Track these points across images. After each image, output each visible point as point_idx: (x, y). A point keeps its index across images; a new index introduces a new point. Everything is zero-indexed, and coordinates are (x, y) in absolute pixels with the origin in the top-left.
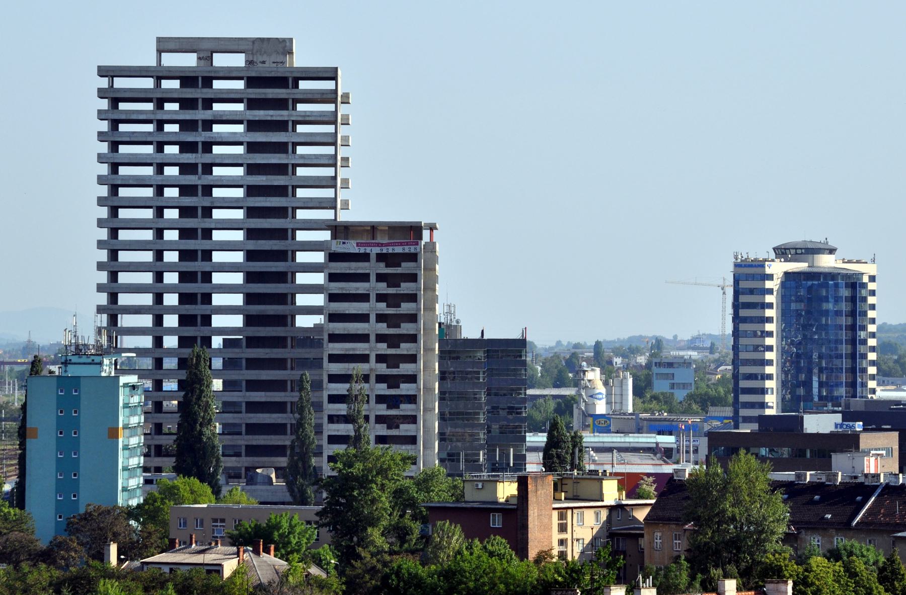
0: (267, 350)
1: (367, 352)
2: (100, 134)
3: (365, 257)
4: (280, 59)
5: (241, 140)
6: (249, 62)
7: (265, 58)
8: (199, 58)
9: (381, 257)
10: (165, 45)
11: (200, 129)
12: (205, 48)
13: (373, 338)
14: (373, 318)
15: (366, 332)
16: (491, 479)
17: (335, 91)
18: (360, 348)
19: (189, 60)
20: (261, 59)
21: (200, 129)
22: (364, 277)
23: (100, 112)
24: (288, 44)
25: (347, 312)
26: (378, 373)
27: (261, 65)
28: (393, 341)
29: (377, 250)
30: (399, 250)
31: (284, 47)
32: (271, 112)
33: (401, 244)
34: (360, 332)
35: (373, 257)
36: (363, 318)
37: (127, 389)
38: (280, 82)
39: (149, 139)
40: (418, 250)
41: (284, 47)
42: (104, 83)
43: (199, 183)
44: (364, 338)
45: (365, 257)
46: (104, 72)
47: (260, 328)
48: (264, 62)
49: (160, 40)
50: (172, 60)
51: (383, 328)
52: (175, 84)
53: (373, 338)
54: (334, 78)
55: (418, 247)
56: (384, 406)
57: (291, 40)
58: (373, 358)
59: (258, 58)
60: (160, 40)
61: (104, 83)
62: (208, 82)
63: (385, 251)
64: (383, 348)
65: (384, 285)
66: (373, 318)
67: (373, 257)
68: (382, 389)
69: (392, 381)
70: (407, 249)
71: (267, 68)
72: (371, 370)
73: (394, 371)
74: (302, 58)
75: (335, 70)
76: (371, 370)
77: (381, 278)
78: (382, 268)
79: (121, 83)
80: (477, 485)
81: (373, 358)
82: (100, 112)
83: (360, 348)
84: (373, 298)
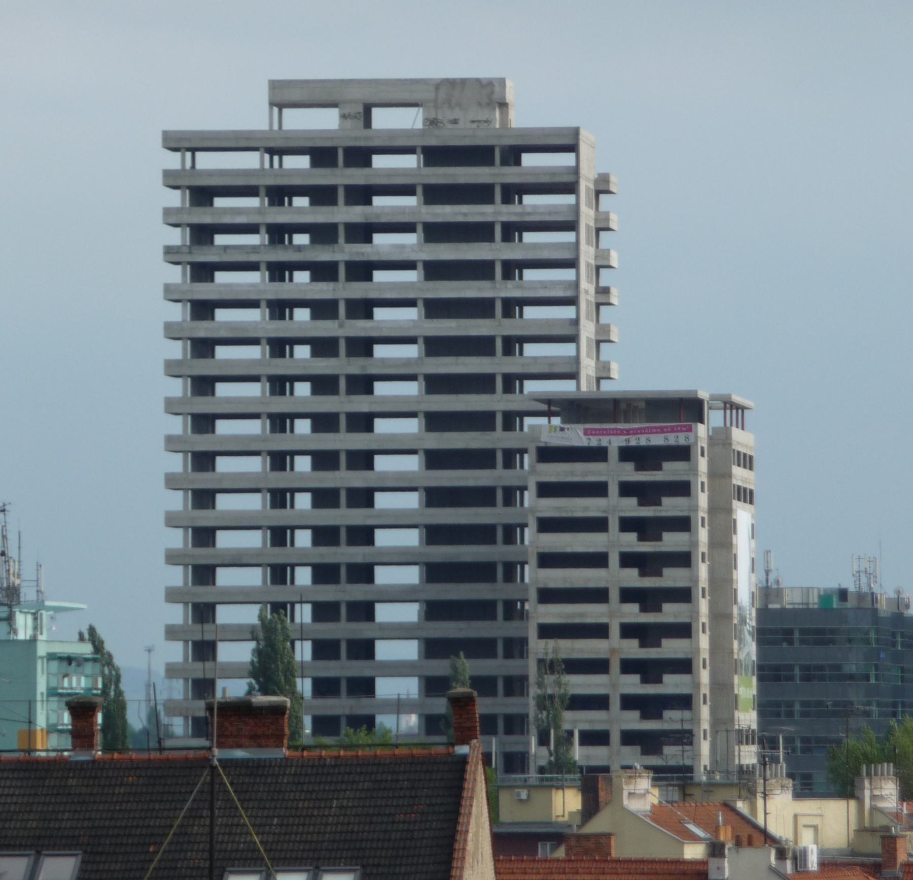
0: (462, 625)
1: (604, 620)
2: (169, 251)
3: (598, 454)
4: (483, 115)
5: (413, 257)
6: (432, 122)
8: (343, 117)
9: (626, 454)
10: (284, 96)
11: (342, 239)
13: (614, 595)
15: (602, 585)
16: (545, 783)
17: (576, 171)
18: (591, 613)
19: (324, 122)
20: (450, 115)
21: (342, 239)
24: (497, 88)
25: (569, 550)
26: (624, 656)
27: (450, 126)
30: (657, 440)
31: (491, 94)
33: (662, 430)
34: (592, 585)
35: (613, 454)
36: (598, 560)
37: (54, 664)
38: (479, 155)
40: (692, 440)
41: (491, 94)
42: (174, 161)
44: (599, 595)
45: (598, 454)
46: (176, 142)
47: (449, 586)
48: (455, 122)
49: (275, 85)
53: (614, 595)
54: (572, 148)
55: (691, 435)
56: (636, 714)
57: (502, 82)
58: (615, 631)
59: (445, 114)
60: (275, 85)
61: (174, 161)
62: (360, 156)
63: (633, 443)
64: (632, 613)
65: (633, 501)
67: (613, 454)
69: (649, 670)
71: (463, 131)
73: (651, 653)
74: (526, 114)
75: (576, 132)
76: (613, 651)
77: (627, 489)
79: (207, 161)
80: (519, 794)
82: (167, 212)
83: (591, 613)
84: (614, 524)
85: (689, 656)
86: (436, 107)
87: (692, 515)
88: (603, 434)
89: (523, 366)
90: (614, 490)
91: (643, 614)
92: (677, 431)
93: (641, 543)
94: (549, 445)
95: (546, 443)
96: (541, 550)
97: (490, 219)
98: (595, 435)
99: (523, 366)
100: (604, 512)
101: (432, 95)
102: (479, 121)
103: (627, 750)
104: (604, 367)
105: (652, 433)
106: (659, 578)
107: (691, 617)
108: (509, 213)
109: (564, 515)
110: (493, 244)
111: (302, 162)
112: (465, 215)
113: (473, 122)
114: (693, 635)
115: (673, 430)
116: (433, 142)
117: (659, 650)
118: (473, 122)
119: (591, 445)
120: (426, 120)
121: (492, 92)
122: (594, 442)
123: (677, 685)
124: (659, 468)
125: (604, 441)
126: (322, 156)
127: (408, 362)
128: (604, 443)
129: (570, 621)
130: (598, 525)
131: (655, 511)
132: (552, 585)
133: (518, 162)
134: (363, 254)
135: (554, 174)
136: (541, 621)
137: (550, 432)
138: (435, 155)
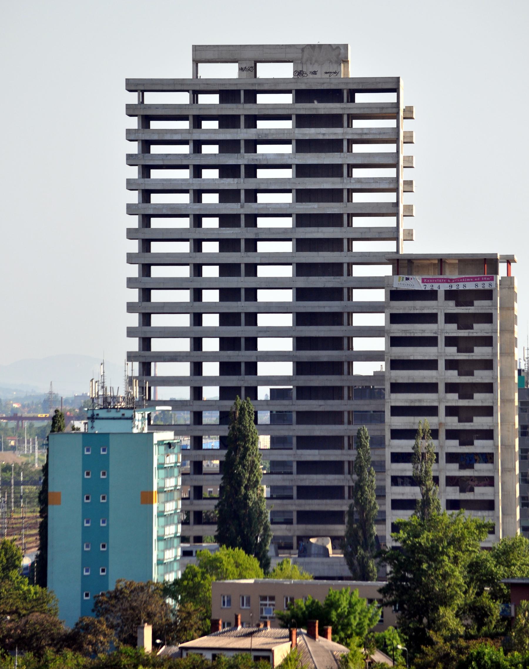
0: (321, 402)
1: (435, 404)
2: (129, 157)
3: (432, 295)
6: (298, 73)
7: (316, 68)
8: (241, 69)
9: (450, 295)
10: (202, 55)
11: (242, 150)
12: (248, 57)
13: (442, 388)
14: (441, 364)
15: (434, 381)
18: (426, 399)
19: (229, 72)
21: (242, 150)
22: (431, 318)
23: (129, 132)
24: (342, 51)
27: (311, 76)
28: (465, 391)
29: (445, 287)
30: (470, 286)
31: (338, 54)
32: (323, 130)
33: (474, 280)
34: (426, 381)
35: (441, 295)
38: (333, 95)
39: (185, 162)
40: (494, 286)
41: (338, 54)
42: (133, 98)
43: (242, 211)
45: (432, 295)
46: (133, 86)
48: (315, 73)
49: (196, 48)
50: (210, 72)
51: (453, 376)
52: (214, 99)
53: (442, 388)
54: (396, 90)
55: (493, 283)
56: (456, 466)
58: (442, 411)
61: (133, 98)
62: (251, 96)
63: (454, 288)
66: (441, 364)
67: (441, 295)
68: (454, 446)
69: (465, 437)
70: (480, 286)
71: (319, 80)
72: (440, 424)
73: (467, 426)
74: (357, 69)
76: (440, 424)
77: (450, 318)
78: (452, 308)
79: (151, 98)
81: (442, 411)
82: (129, 132)
83: (426, 399)
84: (441, 341)
85: (491, 428)
86: (302, 63)
87: (493, 335)
88: (435, 282)
89: (361, 233)
90: (441, 318)
91: (461, 400)
92: (484, 280)
93: (459, 354)
94: (398, 289)
95: (397, 288)
96: (393, 358)
97: (340, 137)
98: (430, 282)
99: (361, 233)
100: (435, 333)
101: (300, 55)
102: (331, 73)
103: (450, 489)
104: (409, 233)
105: (467, 281)
106: (471, 377)
107: (493, 403)
108: (352, 133)
109: (408, 335)
110: (342, 154)
111: (214, 99)
112: (324, 134)
113: (326, 73)
114: (494, 414)
115: (481, 279)
116: (303, 87)
117: (472, 424)
118: (326, 73)
119: (426, 289)
120: (295, 72)
121: (340, 54)
122: (428, 287)
123: (483, 447)
124: (472, 305)
125: (435, 287)
126: (228, 94)
127: (285, 230)
128: (435, 288)
129: (413, 405)
130: (431, 341)
131: (469, 333)
132: (400, 381)
133: (255, 101)
134: (256, 160)
135: (383, 108)
136: (393, 404)
137: (399, 281)
138: (302, 95)
